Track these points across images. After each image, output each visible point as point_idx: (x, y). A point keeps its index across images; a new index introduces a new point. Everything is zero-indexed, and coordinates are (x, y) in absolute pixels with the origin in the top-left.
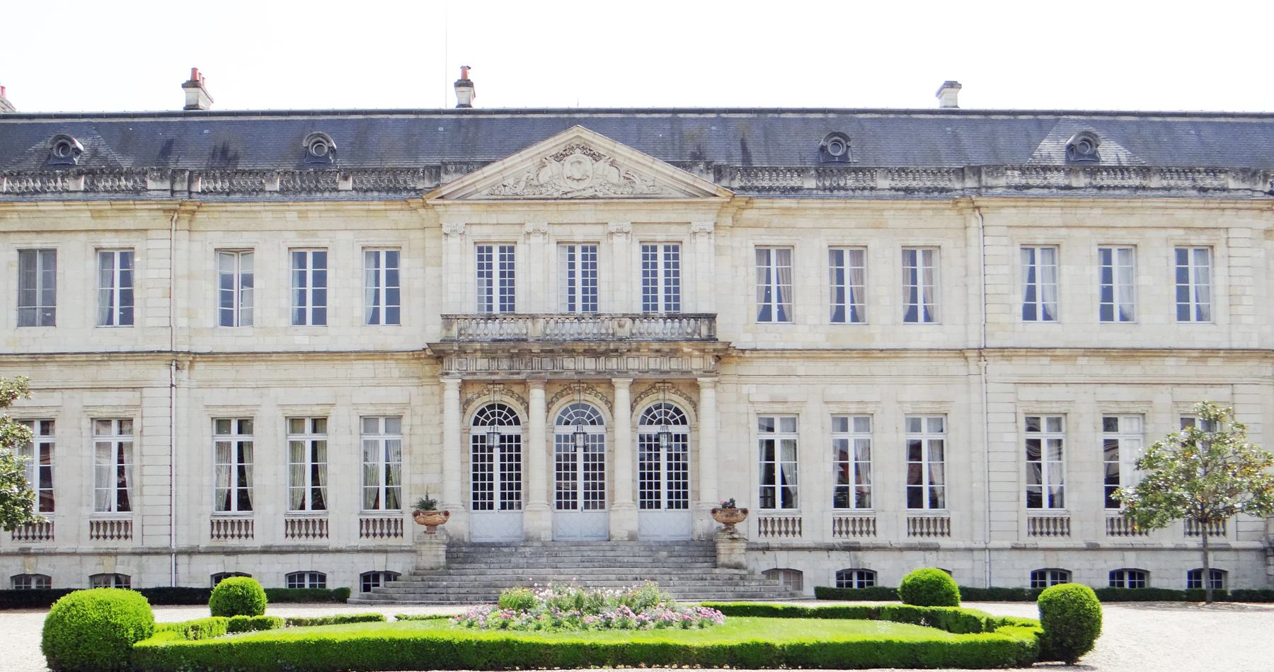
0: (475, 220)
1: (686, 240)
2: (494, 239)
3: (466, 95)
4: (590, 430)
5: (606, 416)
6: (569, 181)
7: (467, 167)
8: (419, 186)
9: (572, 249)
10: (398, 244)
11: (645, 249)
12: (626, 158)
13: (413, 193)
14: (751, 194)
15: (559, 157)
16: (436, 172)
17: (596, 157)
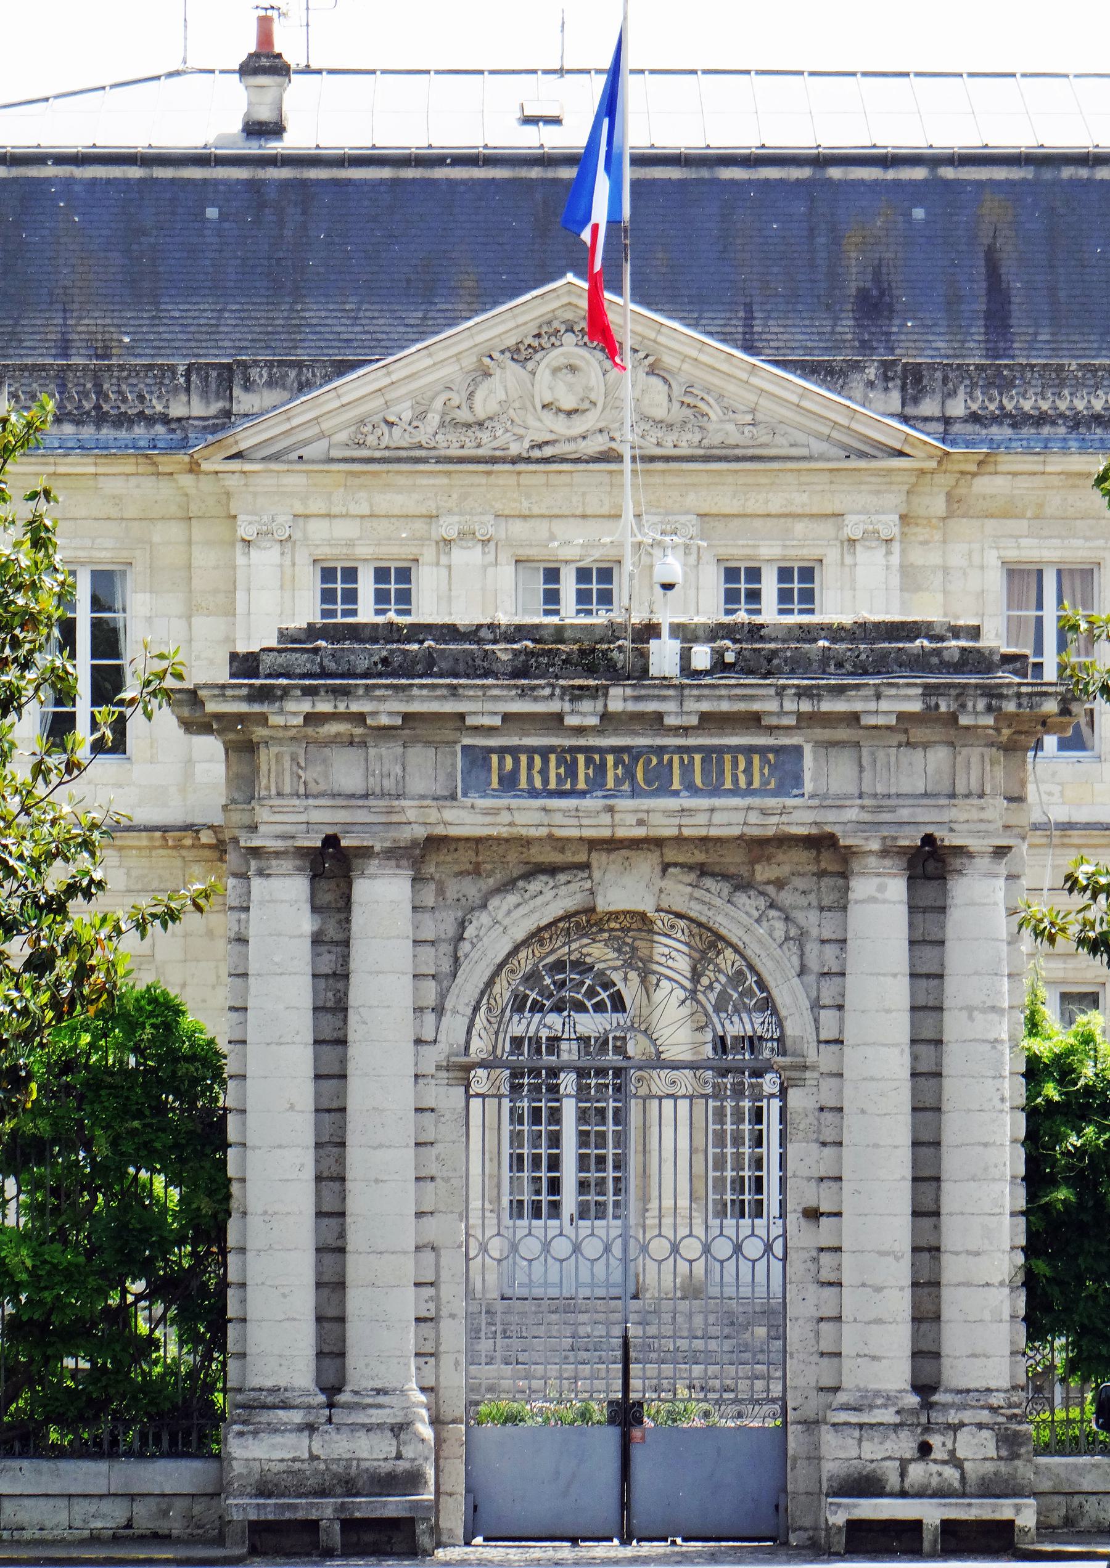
0: (316, 506)
1: (832, 556)
2: (362, 551)
3: (269, 96)
4: (590, 1024)
5: (630, 991)
6: (548, 417)
7: (299, 376)
8: (177, 410)
9: (552, 575)
10: (125, 555)
12: (685, 358)
13: (160, 429)
14: (998, 432)
15: (522, 354)
16: (227, 378)
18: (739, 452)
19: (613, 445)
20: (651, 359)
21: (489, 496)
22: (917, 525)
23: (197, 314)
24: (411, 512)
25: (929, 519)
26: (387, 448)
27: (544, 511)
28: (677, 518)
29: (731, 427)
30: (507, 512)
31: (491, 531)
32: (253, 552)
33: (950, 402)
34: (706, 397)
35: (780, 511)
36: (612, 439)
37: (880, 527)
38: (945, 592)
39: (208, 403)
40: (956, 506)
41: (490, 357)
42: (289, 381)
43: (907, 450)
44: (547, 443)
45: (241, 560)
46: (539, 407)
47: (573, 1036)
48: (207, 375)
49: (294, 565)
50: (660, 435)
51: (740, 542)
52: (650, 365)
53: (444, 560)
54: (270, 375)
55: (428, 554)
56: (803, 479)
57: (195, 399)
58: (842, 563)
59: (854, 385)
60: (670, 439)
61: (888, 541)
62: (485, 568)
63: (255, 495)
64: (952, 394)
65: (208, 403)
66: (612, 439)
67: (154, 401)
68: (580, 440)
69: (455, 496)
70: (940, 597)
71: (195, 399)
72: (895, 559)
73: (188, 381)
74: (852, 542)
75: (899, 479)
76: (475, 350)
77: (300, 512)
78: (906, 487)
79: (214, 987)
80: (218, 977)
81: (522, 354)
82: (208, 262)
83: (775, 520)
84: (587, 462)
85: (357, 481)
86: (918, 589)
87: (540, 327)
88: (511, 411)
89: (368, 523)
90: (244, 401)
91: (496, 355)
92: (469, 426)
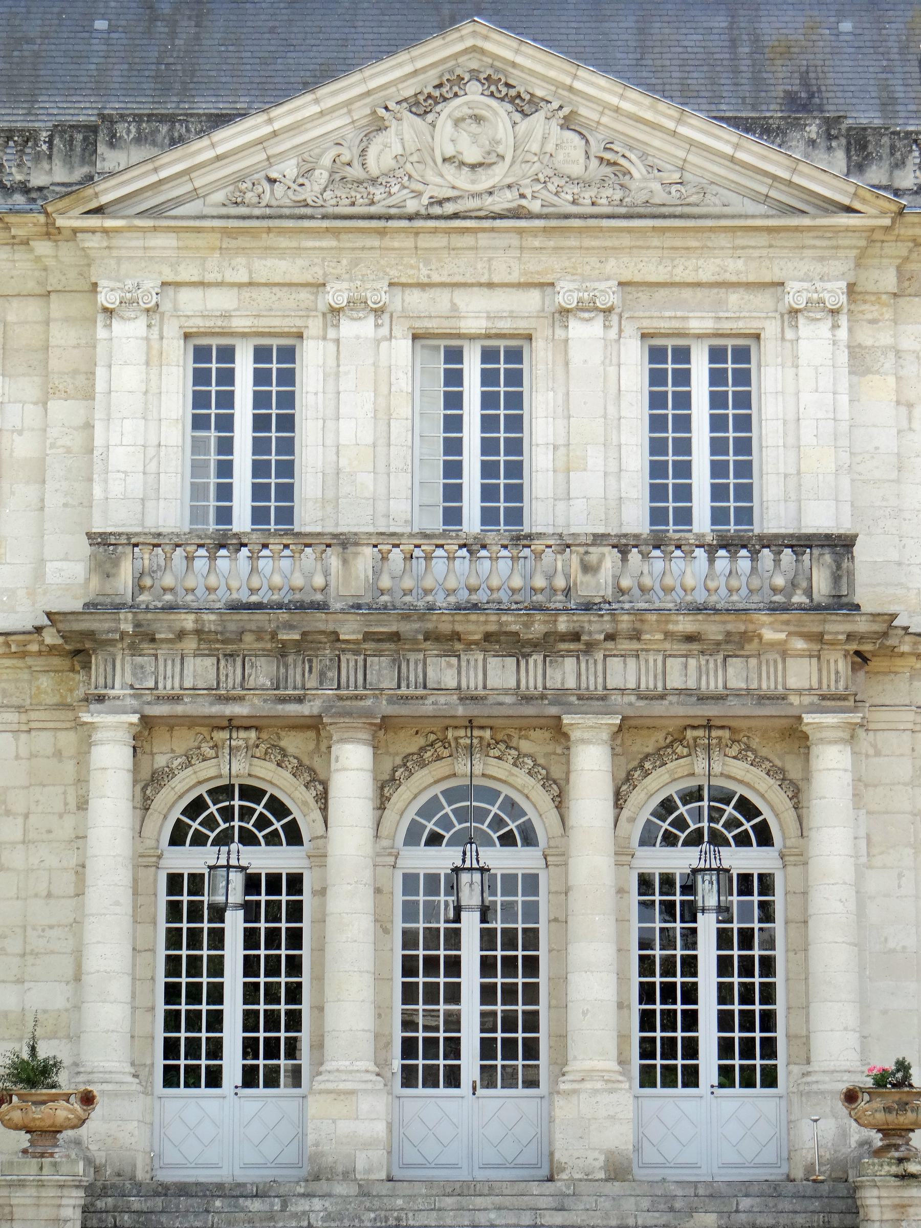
0: (188, 273)
1: (770, 330)
2: (240, 323)
5: (544, 822)
6: (449, 171)
8: (38, 180)
9: (454, 355)
11: (657, 355)
17: (523, 104)
18: (665, 210)
19: (523, 202)
20: (566, 111)
21: (382, 262)
22: (865, 302)
23: (76, 112)
24: (295, 280)
25: (877, 294)
26: (267, 206)
27: (445, 279)
28: (596, 285)
29: (656, 186)
30: (403, 280)
31: (385, 298)
32: (116, 324)
33: (897, 173)
34: (628, 154)
35: (713, 279)
36: (522, 196)
37: (826, 296)
38: (899, 379)
39: (72, 168)
40: (907, 284)
41: (386, 108)
42: (159, 138)
43: (857, 205)
44: (448, 199)
45: (101, 333)
46: (439, 160)
47: (475, 865)
48: (72, 138)
49: (162, 338)
50: (576, 191)
51: (667, 314)
52: (565, 118)
53: (332, 333)
54: (139, 131)
55: (314, 326)
56: (740, 242)
57: (57, 163)
58: (783, 339)
59: (794, 143)
60: (587, 195)
61: (834, 312)
62: (378, 342)
63: (119, 259)
64: (900, 164)
65: (72, 168)
66: (522, 196)
67: (14, 170)
68: (485, 196)
69: (344, 262)
70: (891, 380)
71: (57, 163)
72: (843, 333)
73: (51, 147)
74: (794, 312)
75: (847, 242)
76: (368, 100)
77: (169, 279)
78: (855, 252)
79: (61, 816)
80: (66, 804)
81: (423, 105)
82: (93, 67)
83: (706, 291)
84: (494, 218)
85: (233, 244)
86: (868, 371)
87: (441, 76)
88: (408, 166)
89: (246, 293)
90: (110, 159)
91: (392, 105)
92: (360, 183)
